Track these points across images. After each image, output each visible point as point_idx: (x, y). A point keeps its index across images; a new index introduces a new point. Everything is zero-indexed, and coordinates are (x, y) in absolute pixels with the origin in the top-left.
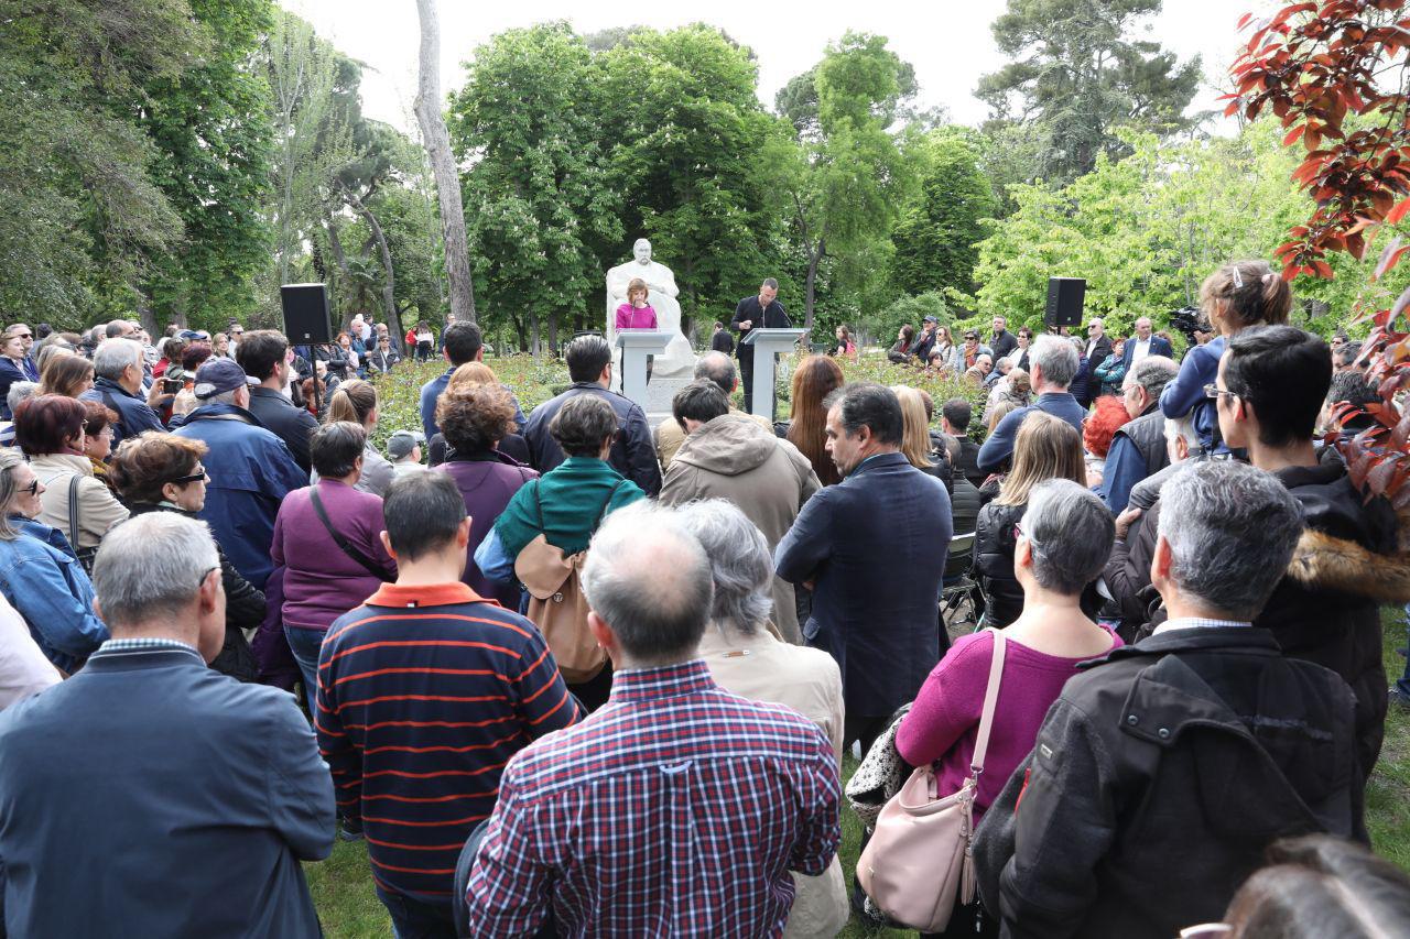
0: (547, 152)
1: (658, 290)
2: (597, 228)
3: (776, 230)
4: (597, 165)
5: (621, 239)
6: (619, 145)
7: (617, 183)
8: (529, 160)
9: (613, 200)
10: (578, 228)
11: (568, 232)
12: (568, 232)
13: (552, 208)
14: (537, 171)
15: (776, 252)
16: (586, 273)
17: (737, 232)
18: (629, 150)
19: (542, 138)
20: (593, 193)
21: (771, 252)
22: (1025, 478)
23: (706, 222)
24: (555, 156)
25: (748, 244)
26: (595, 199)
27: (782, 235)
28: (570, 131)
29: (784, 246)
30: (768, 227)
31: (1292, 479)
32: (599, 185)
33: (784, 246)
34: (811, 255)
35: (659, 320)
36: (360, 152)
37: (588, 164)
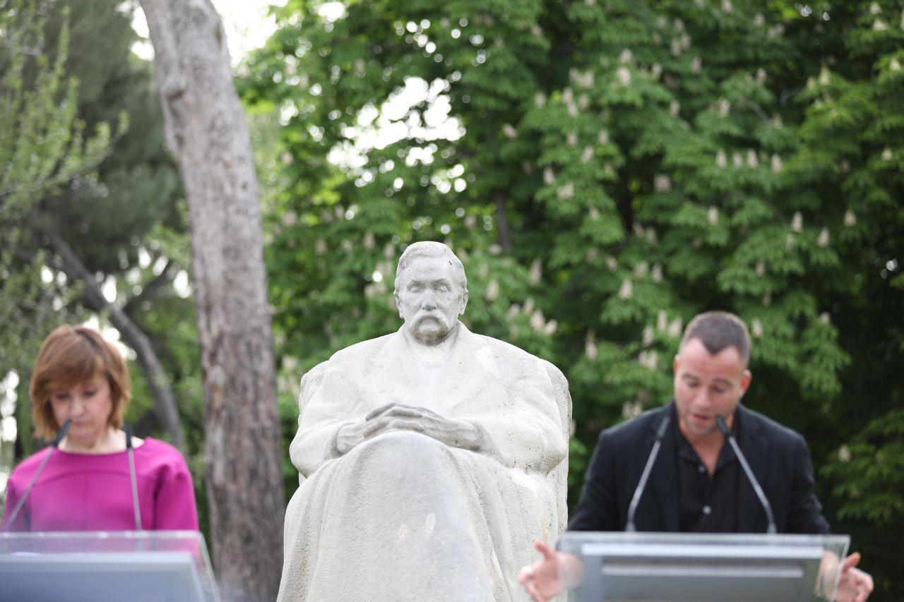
0: (595, 108)
4: (756, 145)
5: (831, 385)
6: (825, 78)
7: (820, 198)
8: (535, 136)
9: (803, 254)
13: (599, 285)
14: (557, 168)
18: (856, 93)
19: (582, 67)
20: (737, 236)
22: (474, 425)
24: (622, 121)
26: (746, 252)
28: (681, 43)
31: (646, 408)
32: (757, 208)
36: (92, 146)
37: (733, 143)
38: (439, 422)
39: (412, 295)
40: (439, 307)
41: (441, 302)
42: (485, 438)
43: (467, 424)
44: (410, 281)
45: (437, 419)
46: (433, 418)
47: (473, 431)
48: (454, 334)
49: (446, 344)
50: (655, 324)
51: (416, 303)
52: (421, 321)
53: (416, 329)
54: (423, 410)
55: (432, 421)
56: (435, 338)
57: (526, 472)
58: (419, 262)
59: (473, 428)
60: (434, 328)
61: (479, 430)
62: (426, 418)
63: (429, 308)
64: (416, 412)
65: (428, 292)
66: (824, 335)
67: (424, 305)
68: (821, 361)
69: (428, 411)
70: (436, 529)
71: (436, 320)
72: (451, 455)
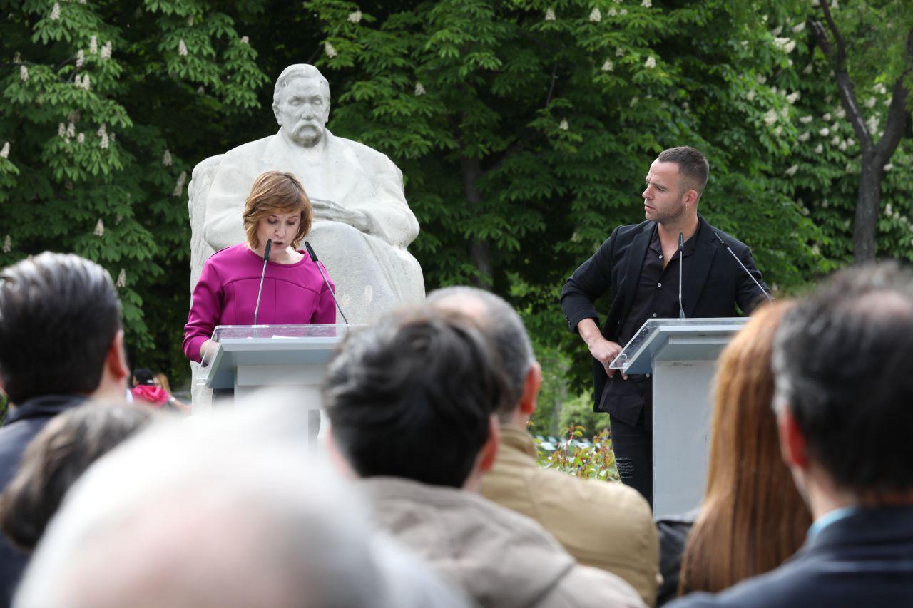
1: (351, 220)
2: (174, 67)
3: (748, 63)
10: (116, 69)
11: (85, 82)
12: (85, 82)
15: (751, 132)
16: (142, 213)
17: (622, 71)
21: (737, 134)
22: (363, 212)
23: (523, 42)
25: (661, 110)
27: (771, 82)
29: (778, 115)
30: (722, 57)
33: (778, 115)
34: (862, 136)
35: (343, 301)
38: (341, 212)
39: (294, 108)
40: (315, 117)
41: (317, 114)
42: (373, 223)
43: (357, 211)
44: (292, 96)
45: (340, 209)
46: (337, 208)
47: (363, 218)
48: (323, 138)
49: (320, 146)
50: (86, 47)
51: (297, 114)
52: (302, 128)
53: (298, 135)
54: (329, 202)
55: (337, 211)
56: (311, 142)
57: (400, 248)
58: (297, 81)
59: (363, 215)
60: (312, 134)
61: (368, 217)
62: (333, 209)
63: (309, 119)
64: (326, 205)
65: (307, 105)
66: (245, 56)
67: (304, 116)
68: (243, 78)
69: (333, 203)
70: (374, 297)
71: (314, 128)
72: (366, 239)
